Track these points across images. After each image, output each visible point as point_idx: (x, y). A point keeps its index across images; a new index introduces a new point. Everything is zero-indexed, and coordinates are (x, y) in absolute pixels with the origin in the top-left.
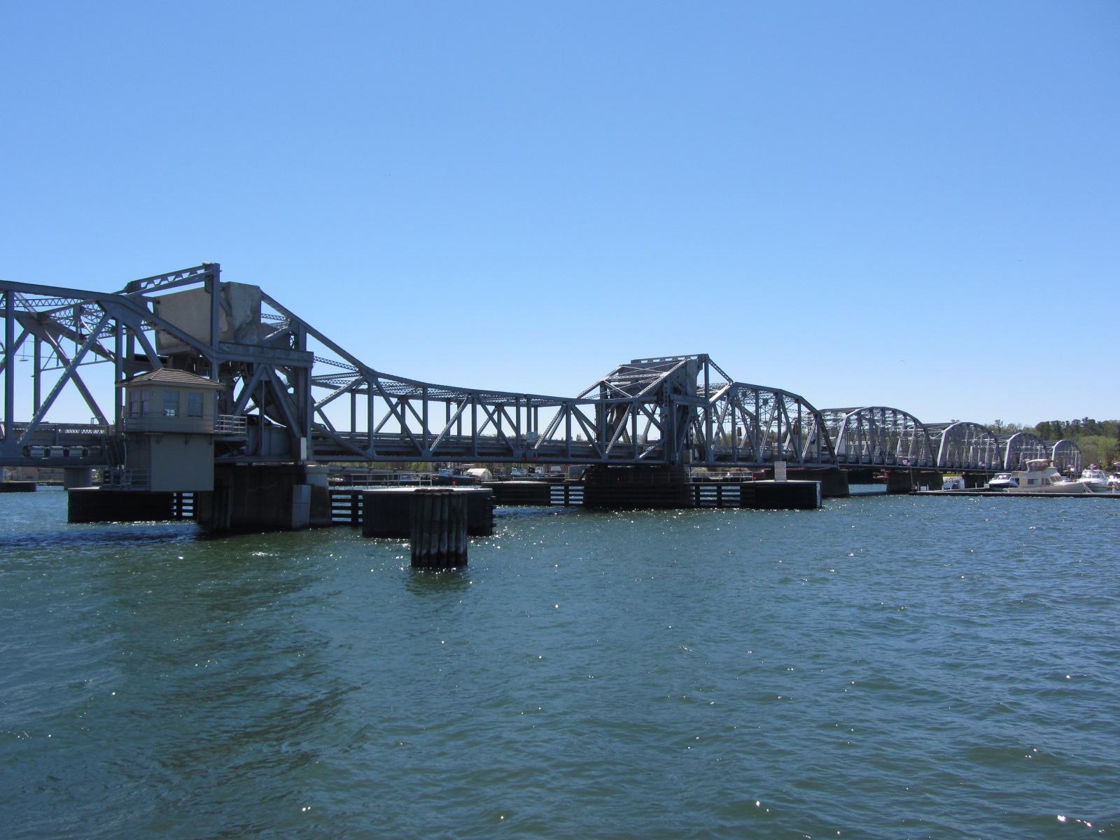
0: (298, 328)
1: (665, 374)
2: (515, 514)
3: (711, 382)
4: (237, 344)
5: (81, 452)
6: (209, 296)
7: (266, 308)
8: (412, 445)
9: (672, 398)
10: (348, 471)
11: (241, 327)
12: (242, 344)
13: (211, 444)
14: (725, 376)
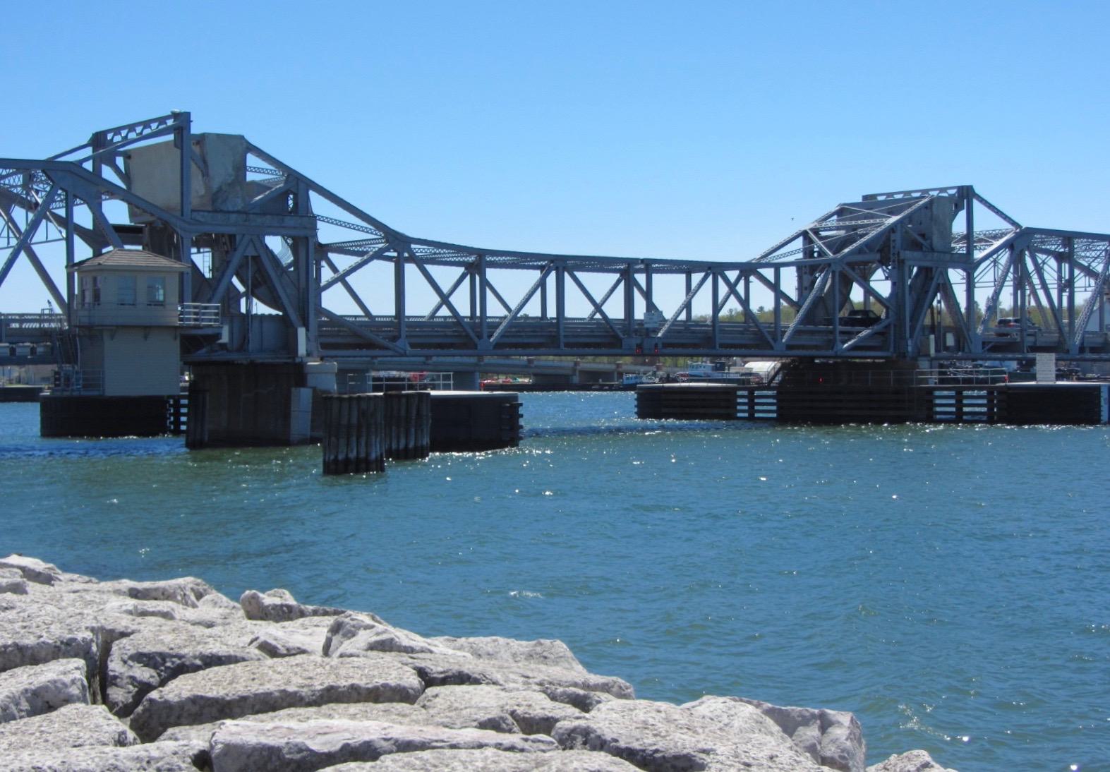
0: (298, 185)
1: (894, 219)
2: (680, 428)
3: (977, 228)
4: (215, 211)
5: (29, 350)
6: (178, 152)
7: (252, 160)
8: (464, 334)
9: (902, 257)
10: (536, 367)
11: (220, 189)
12: (221, 211)
13: (175, 338)
14: (1006, 218)
